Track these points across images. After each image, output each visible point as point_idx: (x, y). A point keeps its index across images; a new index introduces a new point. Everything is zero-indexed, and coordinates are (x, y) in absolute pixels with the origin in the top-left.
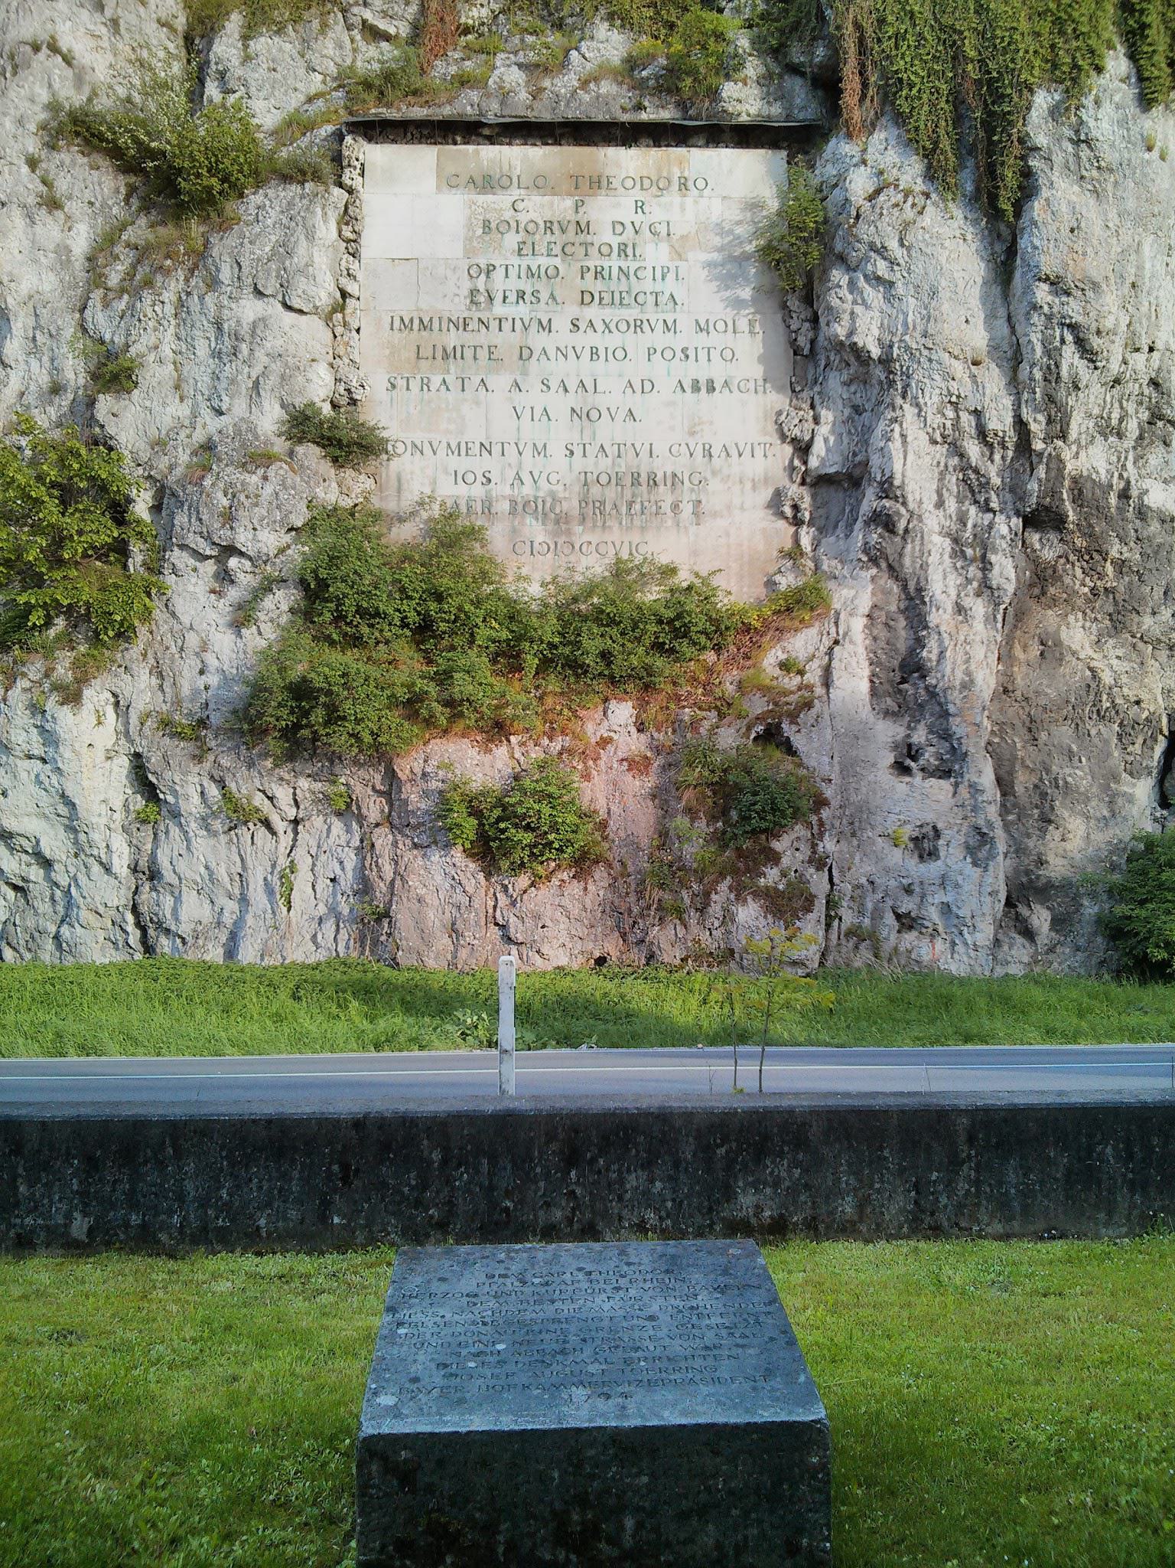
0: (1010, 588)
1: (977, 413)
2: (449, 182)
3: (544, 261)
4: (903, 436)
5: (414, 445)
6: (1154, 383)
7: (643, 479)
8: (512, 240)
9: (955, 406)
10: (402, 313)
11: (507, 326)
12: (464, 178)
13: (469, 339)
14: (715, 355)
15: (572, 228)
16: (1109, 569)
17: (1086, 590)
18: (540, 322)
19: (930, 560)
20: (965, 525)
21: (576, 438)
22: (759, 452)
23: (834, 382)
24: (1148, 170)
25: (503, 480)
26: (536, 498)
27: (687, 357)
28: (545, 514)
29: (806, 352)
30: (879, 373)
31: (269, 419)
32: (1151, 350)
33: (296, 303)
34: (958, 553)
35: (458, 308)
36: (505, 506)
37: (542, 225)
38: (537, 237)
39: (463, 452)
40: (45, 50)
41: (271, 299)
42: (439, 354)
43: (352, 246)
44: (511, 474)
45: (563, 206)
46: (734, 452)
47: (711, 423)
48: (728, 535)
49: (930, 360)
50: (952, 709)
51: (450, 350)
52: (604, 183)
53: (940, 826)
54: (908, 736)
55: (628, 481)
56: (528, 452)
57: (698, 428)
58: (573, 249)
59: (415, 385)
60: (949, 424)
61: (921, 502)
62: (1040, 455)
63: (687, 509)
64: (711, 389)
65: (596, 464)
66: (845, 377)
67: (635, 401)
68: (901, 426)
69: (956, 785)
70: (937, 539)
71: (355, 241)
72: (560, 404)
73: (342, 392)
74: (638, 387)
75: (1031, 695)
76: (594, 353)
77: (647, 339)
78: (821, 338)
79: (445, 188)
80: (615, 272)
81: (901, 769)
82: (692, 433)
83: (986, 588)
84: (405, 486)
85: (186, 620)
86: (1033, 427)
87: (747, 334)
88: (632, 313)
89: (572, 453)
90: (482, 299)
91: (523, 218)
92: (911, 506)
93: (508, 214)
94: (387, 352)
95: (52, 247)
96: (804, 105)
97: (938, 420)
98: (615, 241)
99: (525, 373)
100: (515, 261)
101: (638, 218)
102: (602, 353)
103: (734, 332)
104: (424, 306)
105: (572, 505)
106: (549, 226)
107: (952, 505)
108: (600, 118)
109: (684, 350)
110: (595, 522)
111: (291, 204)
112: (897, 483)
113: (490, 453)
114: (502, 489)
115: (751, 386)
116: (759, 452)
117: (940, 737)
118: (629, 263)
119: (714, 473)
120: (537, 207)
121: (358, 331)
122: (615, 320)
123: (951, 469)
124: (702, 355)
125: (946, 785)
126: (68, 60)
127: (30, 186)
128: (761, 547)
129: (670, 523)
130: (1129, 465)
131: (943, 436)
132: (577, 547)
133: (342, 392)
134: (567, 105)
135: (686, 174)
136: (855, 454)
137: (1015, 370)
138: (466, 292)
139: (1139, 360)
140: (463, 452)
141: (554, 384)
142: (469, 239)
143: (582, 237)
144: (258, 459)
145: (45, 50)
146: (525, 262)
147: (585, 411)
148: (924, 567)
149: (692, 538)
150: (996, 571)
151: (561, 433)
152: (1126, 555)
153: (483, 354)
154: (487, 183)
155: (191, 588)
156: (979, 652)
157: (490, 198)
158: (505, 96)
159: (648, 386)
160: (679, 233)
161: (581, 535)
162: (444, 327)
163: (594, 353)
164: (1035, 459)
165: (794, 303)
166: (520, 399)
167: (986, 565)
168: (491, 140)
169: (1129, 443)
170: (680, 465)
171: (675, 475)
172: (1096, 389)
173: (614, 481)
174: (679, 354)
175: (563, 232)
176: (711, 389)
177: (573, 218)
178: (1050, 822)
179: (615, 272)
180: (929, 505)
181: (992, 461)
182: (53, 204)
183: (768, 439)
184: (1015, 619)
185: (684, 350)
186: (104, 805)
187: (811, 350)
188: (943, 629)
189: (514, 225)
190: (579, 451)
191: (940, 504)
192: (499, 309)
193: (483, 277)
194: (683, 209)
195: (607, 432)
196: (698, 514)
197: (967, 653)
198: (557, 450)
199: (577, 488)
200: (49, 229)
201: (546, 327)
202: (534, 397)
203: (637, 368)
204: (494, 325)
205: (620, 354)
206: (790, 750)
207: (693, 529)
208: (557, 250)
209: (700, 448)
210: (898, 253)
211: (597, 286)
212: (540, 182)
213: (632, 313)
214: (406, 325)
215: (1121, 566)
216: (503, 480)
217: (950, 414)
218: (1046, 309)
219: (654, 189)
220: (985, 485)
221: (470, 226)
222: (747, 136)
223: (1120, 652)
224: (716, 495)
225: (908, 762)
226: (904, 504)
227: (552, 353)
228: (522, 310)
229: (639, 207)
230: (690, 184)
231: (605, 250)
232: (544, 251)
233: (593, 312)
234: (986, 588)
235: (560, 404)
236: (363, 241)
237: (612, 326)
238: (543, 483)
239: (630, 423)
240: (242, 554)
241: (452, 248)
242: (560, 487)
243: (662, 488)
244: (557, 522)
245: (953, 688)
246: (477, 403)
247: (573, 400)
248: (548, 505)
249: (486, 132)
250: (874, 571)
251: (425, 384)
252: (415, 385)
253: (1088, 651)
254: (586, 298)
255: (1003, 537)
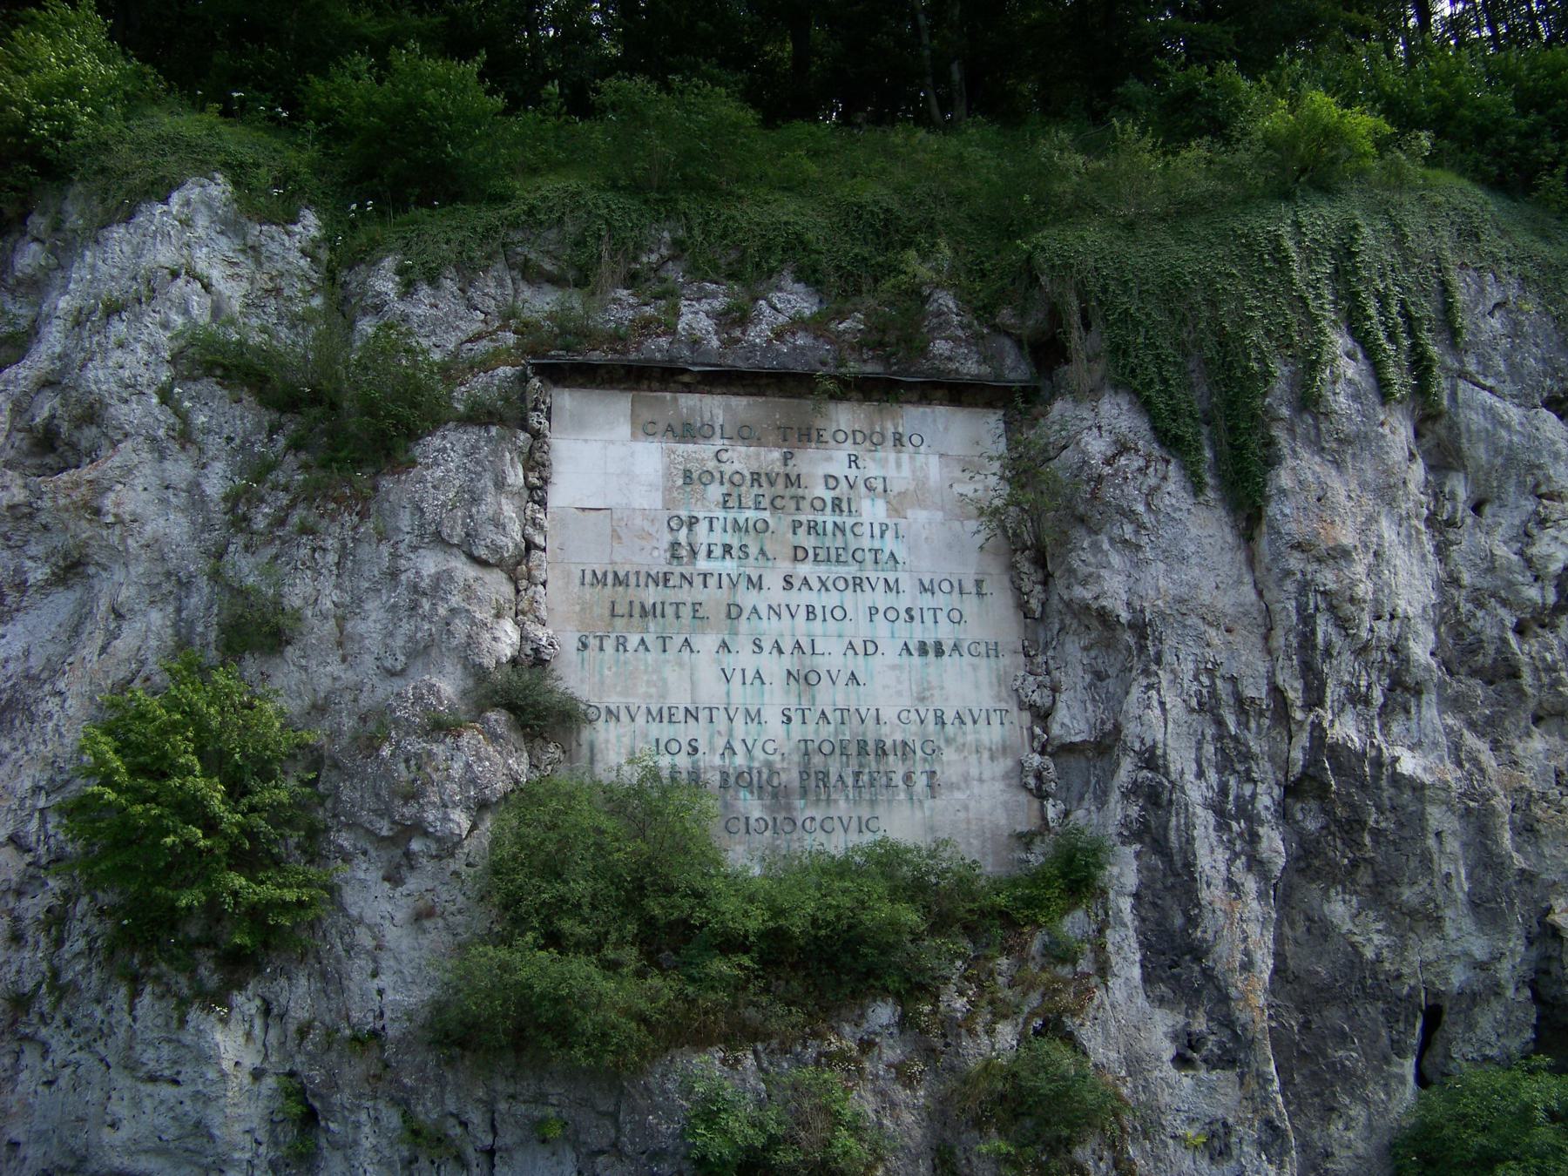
0: (1281, 862)
1: (1233, 680)
2: (644, 429)
3: (751, 514)
4: (1162, 704)
5: (609, 711)
6: (1393, 650)
7: (871, 747)
8: (715, 492)
9: (1210, 673)
10: (595, 567)
11: (712, 582)
12: (661, 426)
13: (671, 595)
14: (941, 616)
15: (781, 481)
16: (1367, 839)
17: (1346, 861)
18: (750, 578)
19: (1196, 833)
20: (1227, 796)
21: (793, 702)
22: (995, 719)
23: (1073, 648)
24: (1382, 443)
25: (712, 749)
26: (750, 769)
27: (912, 618)
28: (760, 787)
29: (1037, 615)
30: (1129, 638)
31: (448, 686)
32: (1392, 617)
33: (482, 553)
34: (1222, 826)
35: (658, 561)
36: (716, 778)
37: (748, 477)
38: (743, 489)
39: (666, 719)
40: (183, 276)
41: (455, 550)
42: (637, 610)
43: (536, 493)
44: (721, 743)
45: (771, 457)
46: (968, 720)
47: (942, 688)
48: (966, 808)
49: (1185, 626)
50: (1233, 992)
51: (648, 607)
52: (814, 435)
53: (1230, 1120)
54: (1188, 1024)
55: (853, 749)
56: (739, 720)
57: (927, 694)
58: (784, 502)
59: (609, 645)
60: (1205, 691)
61: (1182, 772)
62: (1301, 724)
63: (921, 781)
64: (939, 652)
65: (817, 732)
66: (1085, 642)
67: (859, 664)
68: (1159, 692)
69: (1242, 1076)
70: (1199, 810)
71: (540, 488)
72: (774, 667)
73: (529, 652)
74: (860, 649)
75: (1302, 974)
76: (810, 612)
77: (867, 598)
78: (1055, 600)
79: (640, 433)
80: (830, 527)
81: (1181, 1061)
82: (922, 699)
83: (1256, 864)
84: (599, 757)
85: (354, 911)
86: (1291, 695)
87: (974, 598)
88: (850, 570)
89: (789, 719)
90: (684, 553)
91: (728, 469)
92: (1173, 776)
93: (711, 465)
94: (577, 608)
95: (183, 486)
96: (1016, 369)
97: (1195, 687)
98: (828, 496)
99: (734, 633)
100: (721, 514)
101: (852, 473)
102: (819, 611)
103: (961, 593)
104: (618, 558)
105: (791, 777)
106: (756, 478)
107: (1212, 776)
108: (799, 369)
109: (908, 611)
110: (818, 795)
111: (475, 448)
112: (1159, 752)
113: (697, 719)
114: (711, 760)
115: (982, 649)
116: (995, 719)
117: (1221, 1024)
118: (845, 518)
119: (948, 741)
120: (740, 459)
121: (544, 584)
122: (833, 577)
123: (1209, 738)
124: (928, 616)
125: (1231, 1075)
126: (207, 287)
127: (162, 418)
128: (1003, 822)
129: (902, 796)
130: (1377, 733)
131: (1199, 703)
132: (799, 823)
133: (529, 652)
134: (764, 356)
135: (900, 430)
136: (1103, 723)
137: (1266, 638)
138: (666, 545)
139: (1382, 628)
140: (666, 719)
141: (767, 645)
142: (668, 490)
143: (793, 491)
144: (440, 727)
145: (183, 276)
146: (731, 515)
147: (802, 673)
148: (1190, 840)
149: (927, 813)
150: (1264, 844)
151: (776, 698)
152: (1383, 825)
153: (686, 612)
154: (687, 432)
155: (361, 875)
156: (1253, 929)
157: (691, 447)
158: (695, 343)
159: (871, 649)
160: (896, 490)
161: (804, 810)
162: (642, 580)
163: (810, 612)
164: (1294, 727)
165: (1026, 567)
166: (728, 660)
167: (1254, 838)
168: (689, 388)
169: (1374, 711)
170: (911, 733)
171: (905, 744)
172: (1347, 656)
173: (838, 751)
174: (903, 615)
175: (772, 484)
176: (939, 652)
177: (782, 470)
178: (1332, 1109)
179: (830, 527)
180: (1189, 777)
181: (1249, 729)
182: (185, 436)
183: (1003, 706)
184: (1283, 896)
185: (908, 611)
186: (248, 1137)
187: (1043, 612)
188: (1217, 905)
189: (717, 475)
190: (796, 718)
191: (1200, 774)
192: (703, 564)
193: (684, 530)
194: (899, 465)
195: (829, 697)
196: (933, 788)
197: (1243, 931)
198: (773, 717)
199: (796, 758)
200: (180, 469)
201: (756, 584)
202: (744, 658)
203: (859, 628)
204: (698, 581)
205: (838, 614)
206: (1070, 1039)
207: (928, 803)
208: (765, 503)
209: (931, 713)
210: (1147, 519)
211: (809, 542)
212: (746, 432)
213: (850, 570)
214: (599, 580)
215: (1377, 834)
216: (712, 749)
217: (1205, 680)
218: (1299, 576)
219: (867, 444)
220: (1247, 756)
221: (668, 475)
222: (959, 393)
223: (1380, 926)
224: (951, 764)
225: (1190, 1053)
226: (1166, 774)
227: (763, 611)
228: (729, 566)
229: (853, 461)
230: (905, 440)
231: (818, 504)
232: (751, 504)
233: (804, 569)
234: (1256, 864)
235: (774, 667)
236: (551, 490)
237: (829, 584)
238: (758, 753)
239: (852, 687)
240: (426, 834)
241: (646, 497)
242: (777, 758)
243: (891, 758)
244: (775, 796)
245: (1232, 970)
246: (681, 665)
247: (787, 662)
248: (765, 776)
249: (686, 378)
250: (1137, 847)
251: (621, 644)
252: (609, 645)
253: (1347, 926)
254: (798, 554)
255: (1267, 808)
